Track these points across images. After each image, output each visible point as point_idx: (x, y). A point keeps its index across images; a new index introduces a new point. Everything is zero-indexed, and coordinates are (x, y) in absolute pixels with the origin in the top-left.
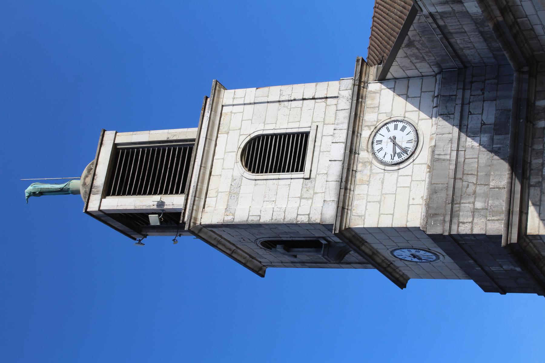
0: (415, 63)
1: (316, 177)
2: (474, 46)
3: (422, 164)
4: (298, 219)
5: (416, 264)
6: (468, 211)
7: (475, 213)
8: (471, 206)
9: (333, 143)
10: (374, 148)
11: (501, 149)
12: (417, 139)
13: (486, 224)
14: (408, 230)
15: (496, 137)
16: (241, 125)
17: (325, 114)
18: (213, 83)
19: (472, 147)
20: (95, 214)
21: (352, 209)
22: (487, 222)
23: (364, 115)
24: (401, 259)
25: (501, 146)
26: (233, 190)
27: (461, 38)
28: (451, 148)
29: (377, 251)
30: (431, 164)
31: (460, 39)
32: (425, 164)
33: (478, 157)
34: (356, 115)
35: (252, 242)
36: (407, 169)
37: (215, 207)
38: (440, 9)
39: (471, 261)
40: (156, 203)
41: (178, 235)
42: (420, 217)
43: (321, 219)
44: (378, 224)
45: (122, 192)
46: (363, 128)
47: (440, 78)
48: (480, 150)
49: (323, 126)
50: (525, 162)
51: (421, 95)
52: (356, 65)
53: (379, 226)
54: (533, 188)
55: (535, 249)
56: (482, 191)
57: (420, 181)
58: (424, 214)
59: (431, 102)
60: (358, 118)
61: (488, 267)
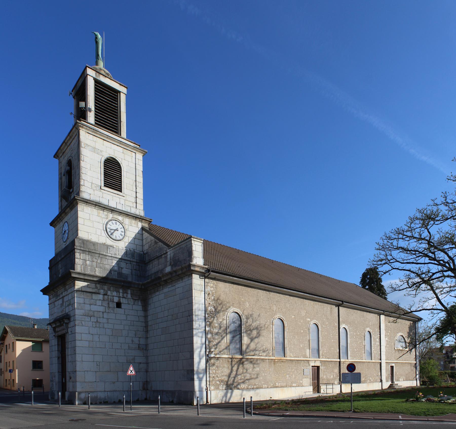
8: (88, 259)
19: (112, 263)
24: (63, 225)
34: (128, 215)
36: (104, 234)
38: (169, 257)
39: (63, 256)
40: (90, 107)
43: (82, 191)
45: (96, 90)
50: (106, 283)
56: (94, 265)
58: (84, 238)
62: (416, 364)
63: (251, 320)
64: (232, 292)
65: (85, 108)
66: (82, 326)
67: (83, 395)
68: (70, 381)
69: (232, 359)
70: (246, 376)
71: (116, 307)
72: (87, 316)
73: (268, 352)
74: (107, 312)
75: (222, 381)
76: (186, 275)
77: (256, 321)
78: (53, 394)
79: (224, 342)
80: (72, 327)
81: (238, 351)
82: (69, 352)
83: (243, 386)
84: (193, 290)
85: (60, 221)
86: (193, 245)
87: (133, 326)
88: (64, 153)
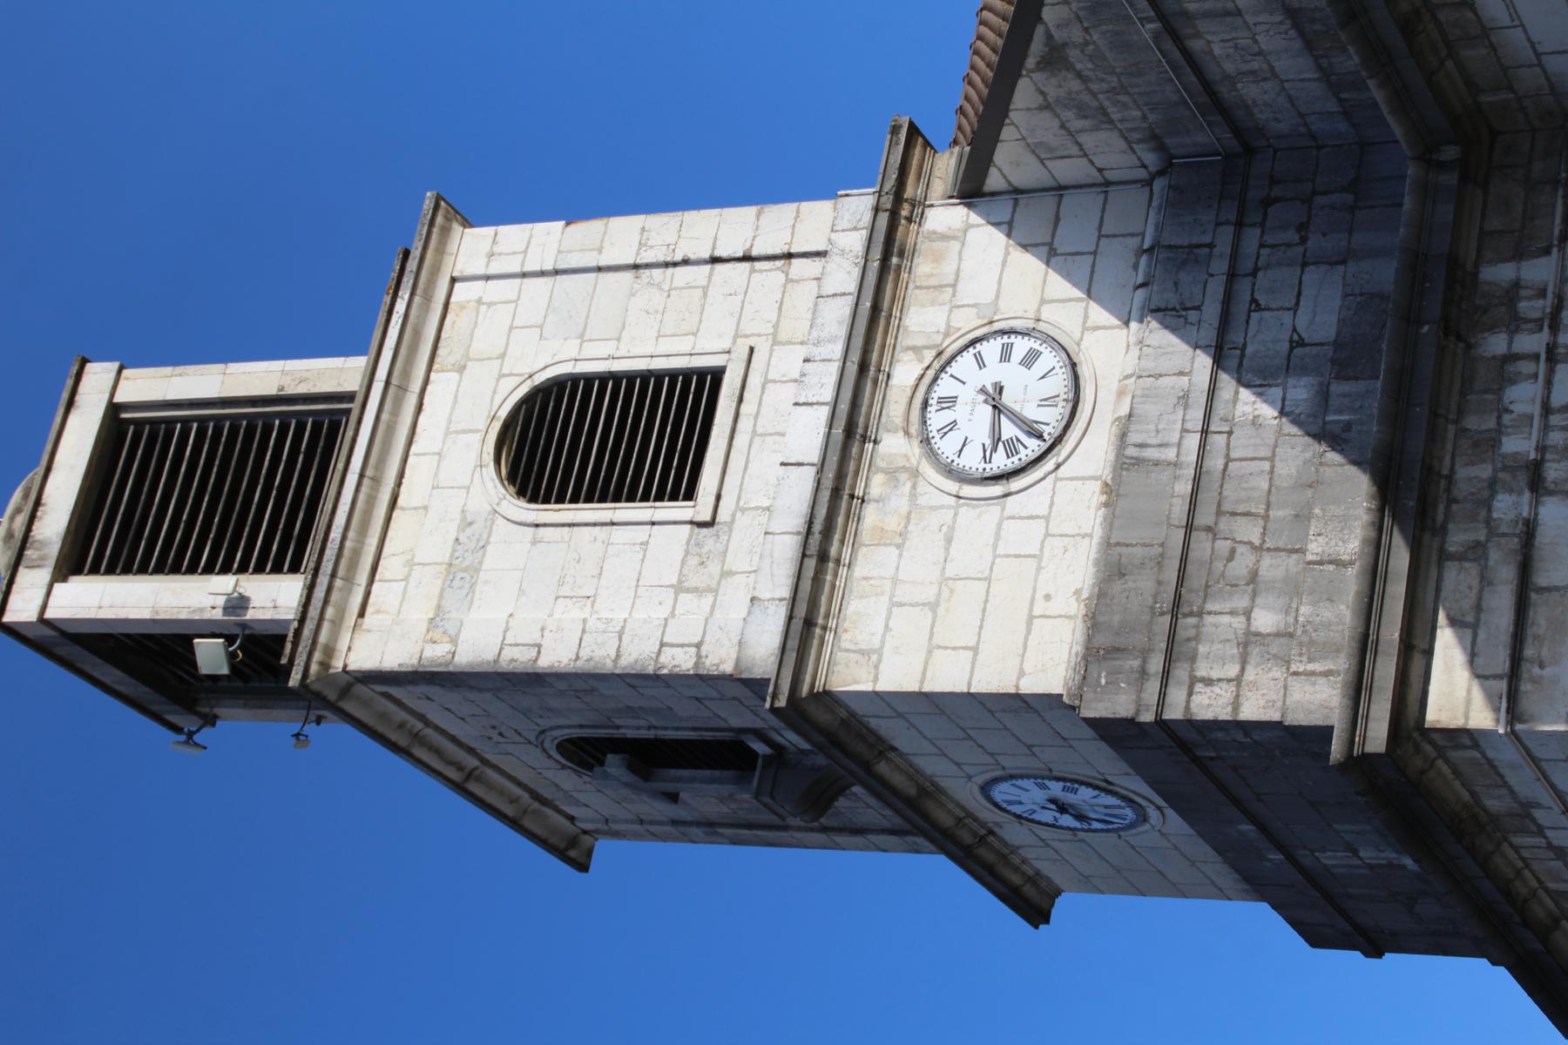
0: (1077, 132)
1: (733, 520)
2: (1272, 69)
3: (1083, 479)
4: (662, 659)
5: (1070, 837)
6: (1228, 640)
7: (1250, 648)
8: (1239, 622)
9: (796, 404)
10: (929, 422)
11: (1354, 429)
12: (1075, 393)
13: (1285, 687)
14: (1024, 705)
15: (1336, 388)
16: (507, 345)
17: (780, 308)
18: (427, 202)
19: (1256, 422)
20: (29, 634)
21: (839, 627)
22: (1290, 679)
23: (905, 310)
24: (1019, 817)
25: (1352, 417)
26: (460, 559)
27: (1227, 37)
28: (1183, 424)
29: (934, 784)
30: (1112, 479)
31: (1222, 41)
32: (1096, 478)
33: (1274, 455)
34: (876, 309)
35: (530, 743)
36: (1033, 495)
37: (399, 612)
39: (1247, 828)
40: (221, 601)
41: (312, 717)
42: (1066, 660)
43: (738, 660)
44: (922, 682)
45: (122, 563)
46: (900, 355)
47: (1163, 189)
48: (1279, 432)
49: (771, 351)
50: (1429, 473)
51: (1097, 246)
52: (887, 144)
53: (927, 688)
54: (1456, 563)
55: (1457, 784)
56: (1279, 573)
57: (1073, 536)
58: (1078, 648)
59: (1131, 269)
60: (882, 322)
61: (1308, 853)
65: (230, 639)
88: (536, 796)
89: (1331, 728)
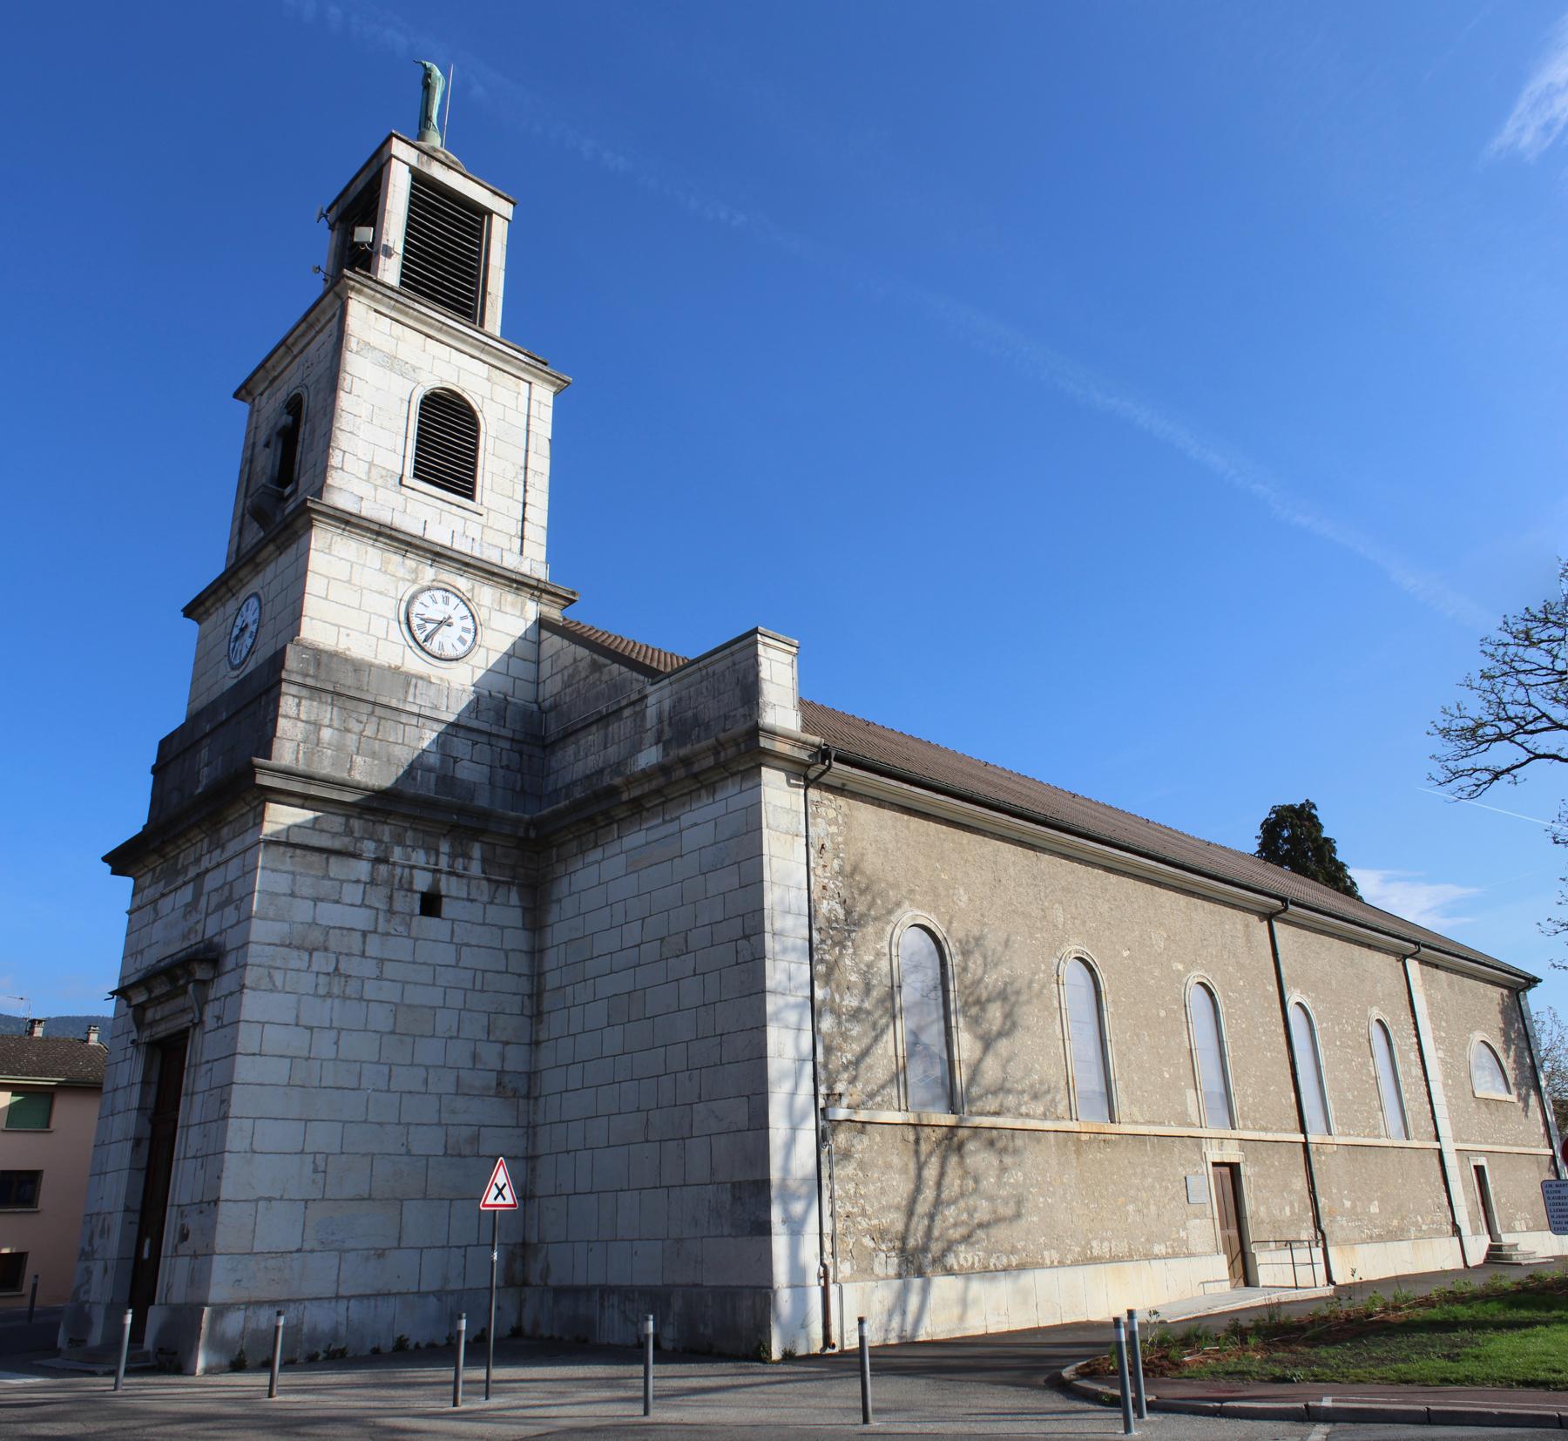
3: (403, 658)
8: (327, 722)
15: (433, 776)
19: (421, 738)
20: (385, 148)
29: (260, 571)
34: (494, 574)
36: (398, 634)
38: (651, 713)
39: (224, 716)
40: (391, 245)
43: (330, 486)
45: (415, 201)
48: (415, 749)
50: (388, 813)
53: (309, 573)
56: (348, 743)
58: (321, 646)
62: (1554, 1157)
63: (980, 961)
64: (905, 846)
65: (371, 245)
66: (271, 991)
67: (233, 1324)
68: (185, 1248)
69: (919, 1128)
70: (975, 1209)
71: (417, 910)
72: (298, 948)
73: (1049, 1097)
74: (379, 930)
75: (881, 1234)
76: (733, 775)
77: (996, 965)
78: (82, 1321)
79: (886, 1051)
80: (226, 996)
81: (939, 1091)
82: (192, 1110)
83: (965, 1258)
84: (765, 831)
85: (230, 594)
86: (761, 659)
87: (482, 991)
88: (275, 379)
89: (270, 759)
